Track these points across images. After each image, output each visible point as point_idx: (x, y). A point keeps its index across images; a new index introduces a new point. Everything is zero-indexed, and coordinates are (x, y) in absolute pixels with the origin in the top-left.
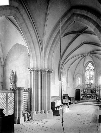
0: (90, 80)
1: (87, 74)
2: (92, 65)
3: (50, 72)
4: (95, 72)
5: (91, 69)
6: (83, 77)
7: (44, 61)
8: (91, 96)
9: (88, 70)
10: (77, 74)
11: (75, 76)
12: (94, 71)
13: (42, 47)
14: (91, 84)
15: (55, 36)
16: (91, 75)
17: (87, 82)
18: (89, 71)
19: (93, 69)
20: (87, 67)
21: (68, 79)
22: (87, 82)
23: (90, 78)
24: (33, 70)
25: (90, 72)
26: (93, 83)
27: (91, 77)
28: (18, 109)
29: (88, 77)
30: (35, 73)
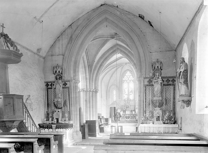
0: (129, 95)
1: (125, 86)
2: (130, 74)
3: (97, 92)
4: (134, 85)
5: (130, 81)
6: (120, 89)
7: (92, 82)
8: (130, 116)
9: (127, 81)
10: (112, 85)
11: (110, 88)
12: (133, 83)
13: (91, 70)
14: (130, 100)
15: (102, 61)
16: (129, 88)
17: (125, 97)
18: (127, 82)
19: (133, 80)
20: (125, 77)
21: (102, 92)
22: (125, 97)
23: (128, 91)
24: (84, 91)
25: (128, 83)
26: (132, 98)
27: (130, 90)
28: (187, 81)
29: (126, 90)
30: (84, 93)
